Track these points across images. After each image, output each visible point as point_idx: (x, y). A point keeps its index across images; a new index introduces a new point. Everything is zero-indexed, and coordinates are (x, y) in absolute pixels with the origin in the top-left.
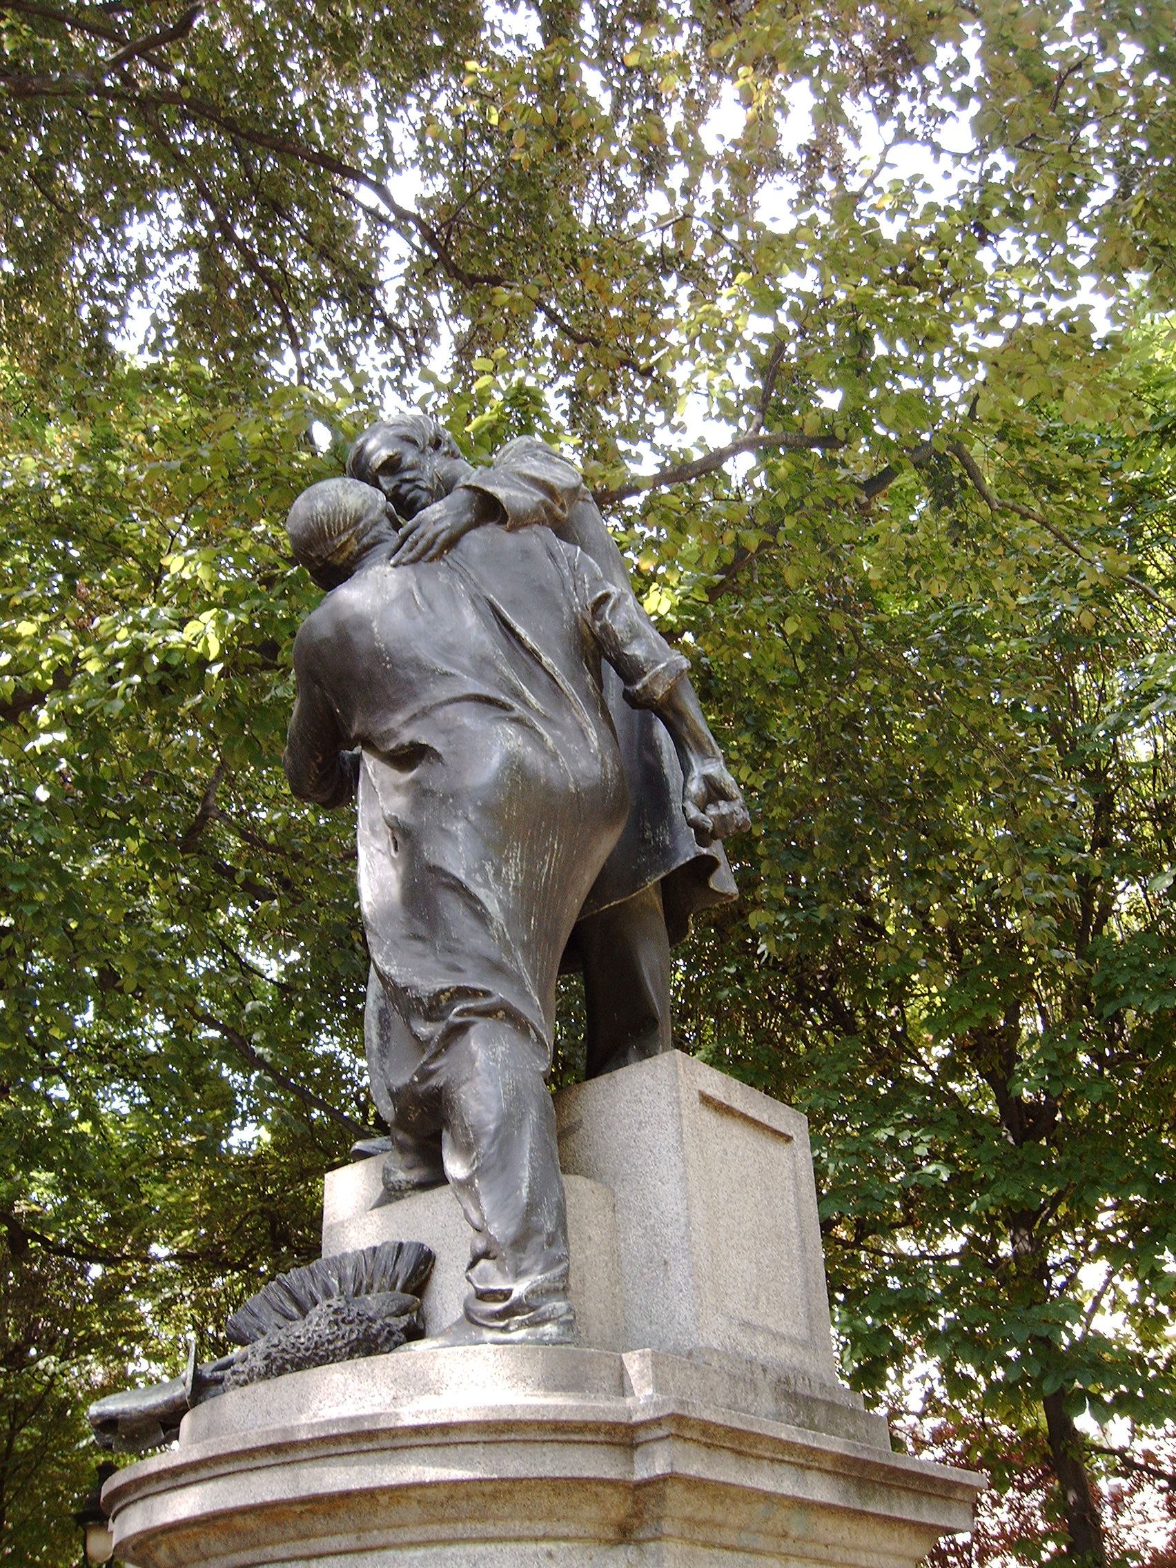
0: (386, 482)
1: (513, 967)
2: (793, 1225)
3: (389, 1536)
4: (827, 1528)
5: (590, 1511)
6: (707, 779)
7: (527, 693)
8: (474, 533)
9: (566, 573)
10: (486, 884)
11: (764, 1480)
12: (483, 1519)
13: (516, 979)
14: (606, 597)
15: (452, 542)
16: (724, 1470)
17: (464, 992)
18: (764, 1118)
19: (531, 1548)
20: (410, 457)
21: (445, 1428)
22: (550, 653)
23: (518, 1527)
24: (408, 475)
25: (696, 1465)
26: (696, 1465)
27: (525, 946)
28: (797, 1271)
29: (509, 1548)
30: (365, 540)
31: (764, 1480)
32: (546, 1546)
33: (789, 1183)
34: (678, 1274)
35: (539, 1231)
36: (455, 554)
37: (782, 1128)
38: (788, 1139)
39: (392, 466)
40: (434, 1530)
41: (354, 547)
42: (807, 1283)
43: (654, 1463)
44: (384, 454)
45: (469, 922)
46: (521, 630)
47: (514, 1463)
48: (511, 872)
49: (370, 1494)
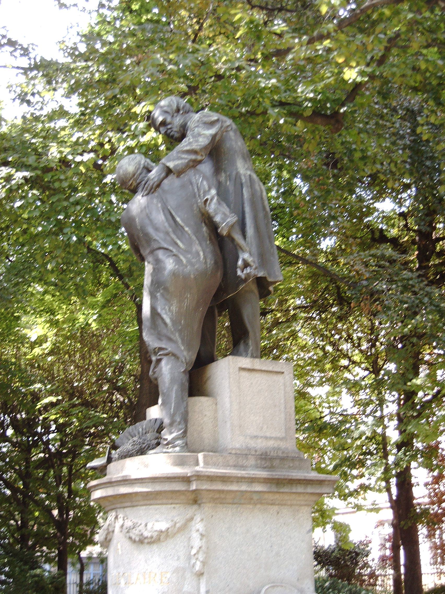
0: (162, 129)
1: (174, 338)
2: (282, 401)
3: (136, 503)
4: (266, 496)
5: (183, 497)
6: (244, 260)
7: (178, 242)
8: (166, 181)
9: (196, 190)
10: (166, 313)
11: (234, 487)
12: (156, 499)
13: (175, 342)
14: (207, 200)
15: (159, 185)
16: (219, 486)
17: (160, 349)
18: (270, 369)
19: (169, 506)
20: (169, 120)
21: (142, 479)
22: (187, 226)
23: (165, 501)
24: (169, 127)
25: (205, 486)
26: (205, 486)
27: (180, 331)
28: (283, 415)
29: (164, 506)
30: (138, 181)
31: (234, 487)
32: (173, 506)
33: (282, 387)
34: (228, 425)
35: (176, 421)
36: (159, 190)
37: (279, 370)
38: (283, 373)
39: (163, 123)
40: (146, 502)
41: (135, 184)
42: (286, 419)
43: (194, 487)
44: (160, 119)
45: (163, 325)
46: (178, 219)
47: (158, 487)
48: (174, 308)
49: (131, 494)
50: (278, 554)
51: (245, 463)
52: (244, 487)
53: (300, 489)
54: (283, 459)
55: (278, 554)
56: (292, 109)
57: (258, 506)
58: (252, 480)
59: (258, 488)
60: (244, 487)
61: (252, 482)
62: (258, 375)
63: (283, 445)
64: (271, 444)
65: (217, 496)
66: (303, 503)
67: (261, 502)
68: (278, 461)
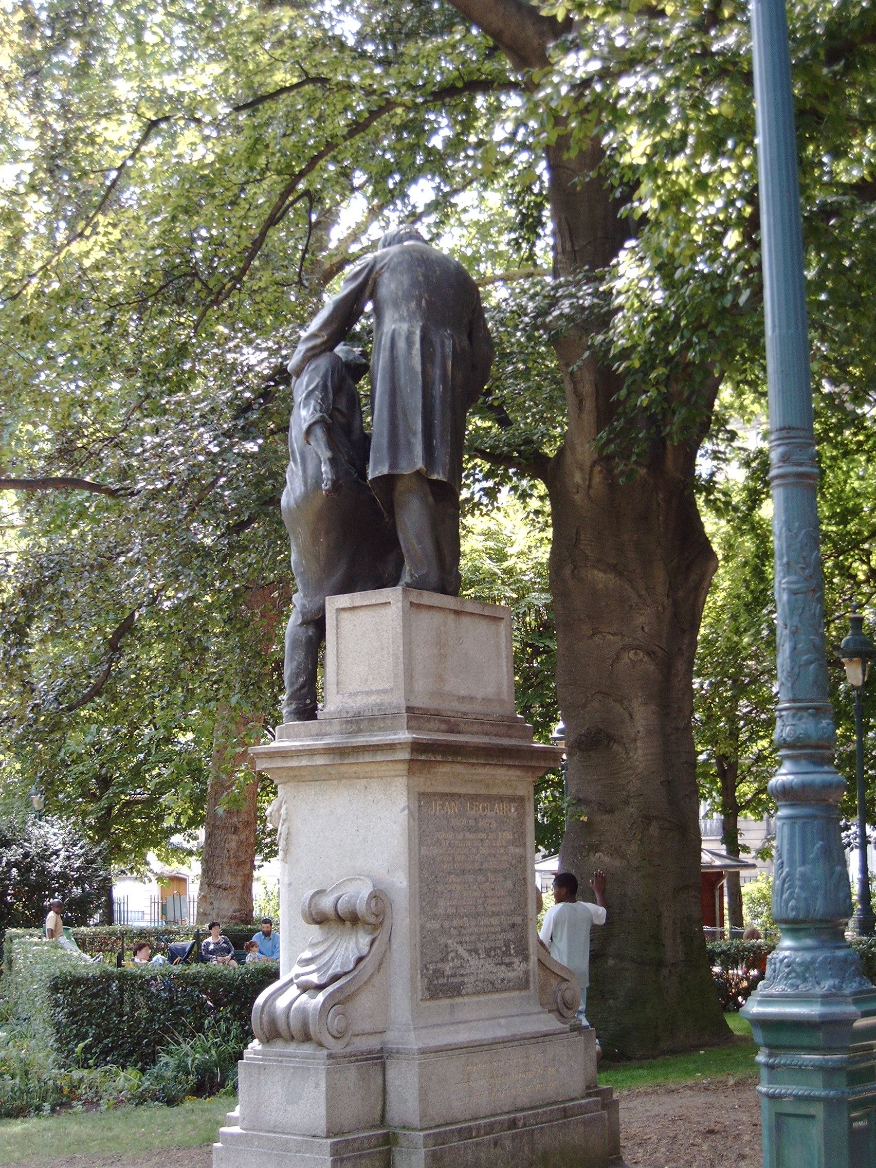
11: (294, 763)
18: (374, 602)
31: (294, 763)
50: (365, 840)
51: (328, 729)
52: (304, 762)
53: (368, 758)
54: (372, 719)
55: (365, 840)
56: (140, 319)
57: (344, 781)
58: (311, 752)
59: (320, 761)
60: (304, 762)
61: (313, 755)
62: (362, 613)
63: (386, 699)
64: (373, 699)
65: (291, 774)
66: (393, 773)
67: (329, 778)
68: (366, 722)
